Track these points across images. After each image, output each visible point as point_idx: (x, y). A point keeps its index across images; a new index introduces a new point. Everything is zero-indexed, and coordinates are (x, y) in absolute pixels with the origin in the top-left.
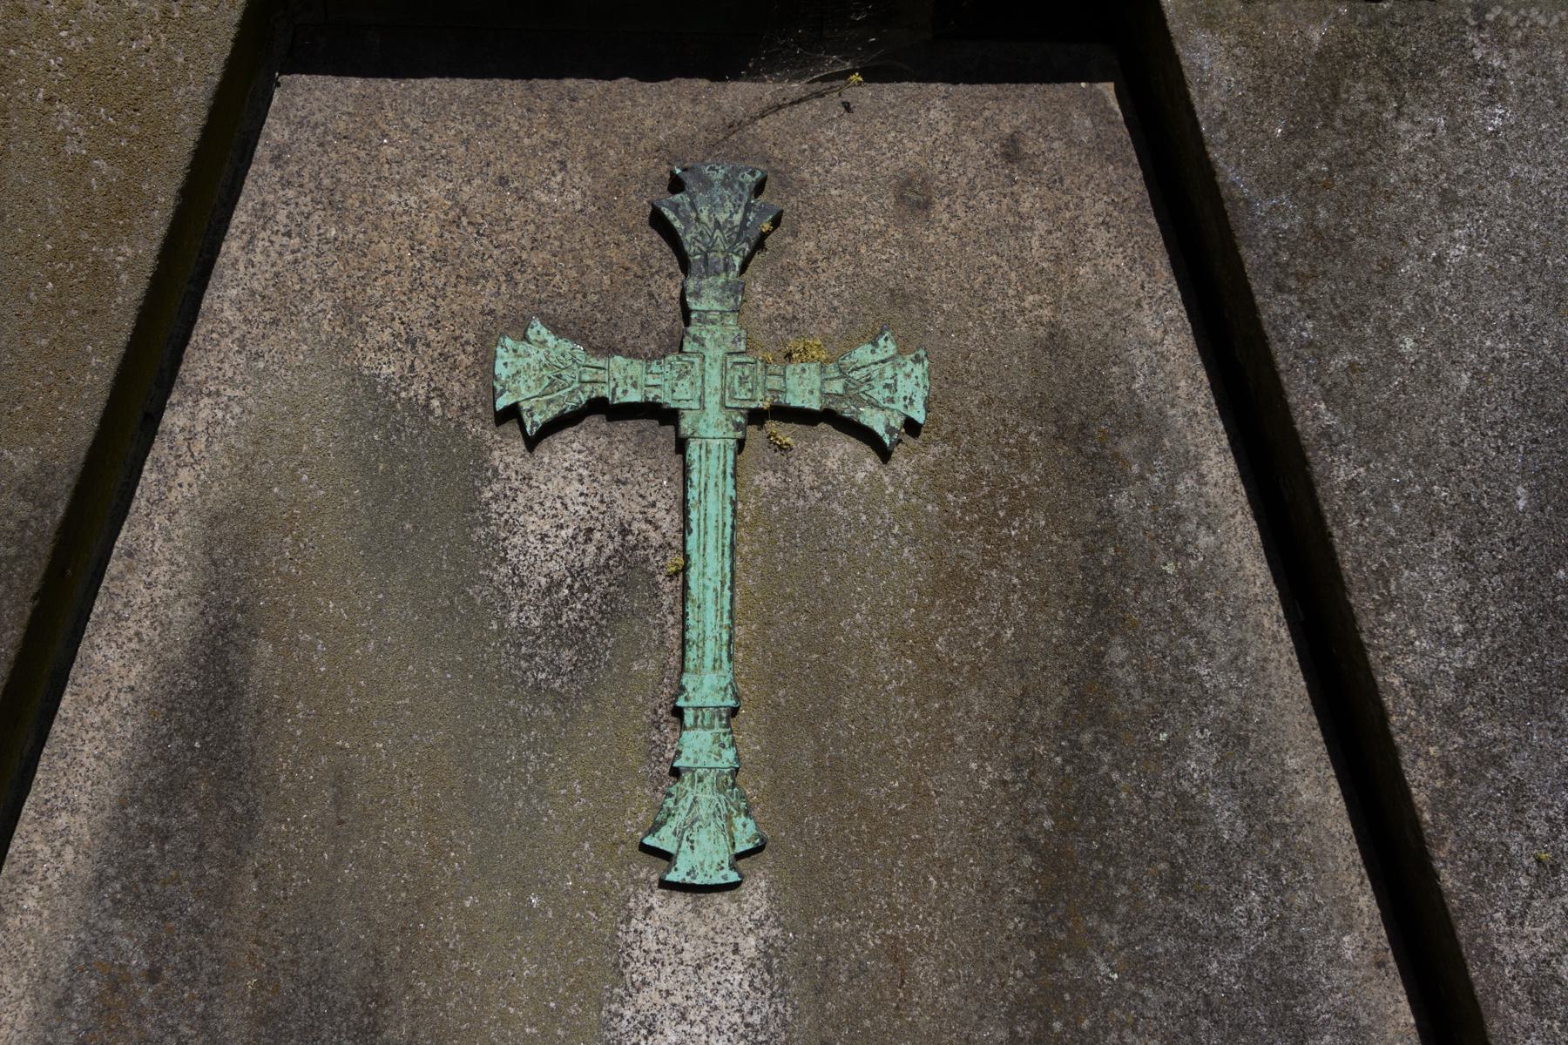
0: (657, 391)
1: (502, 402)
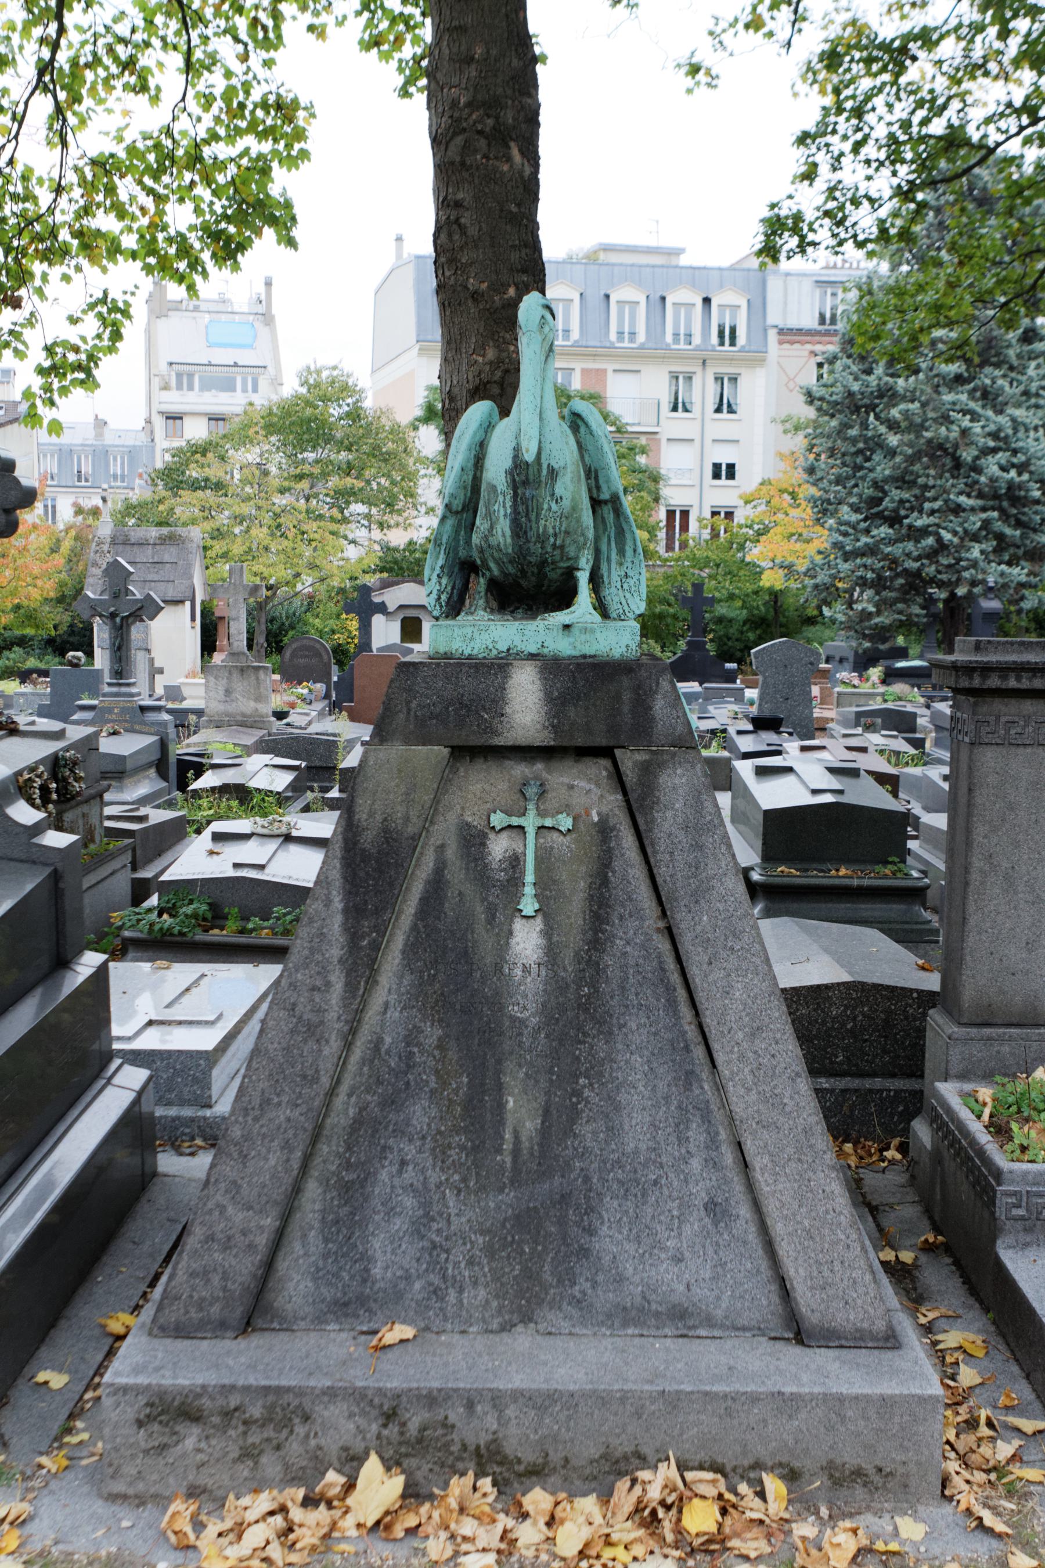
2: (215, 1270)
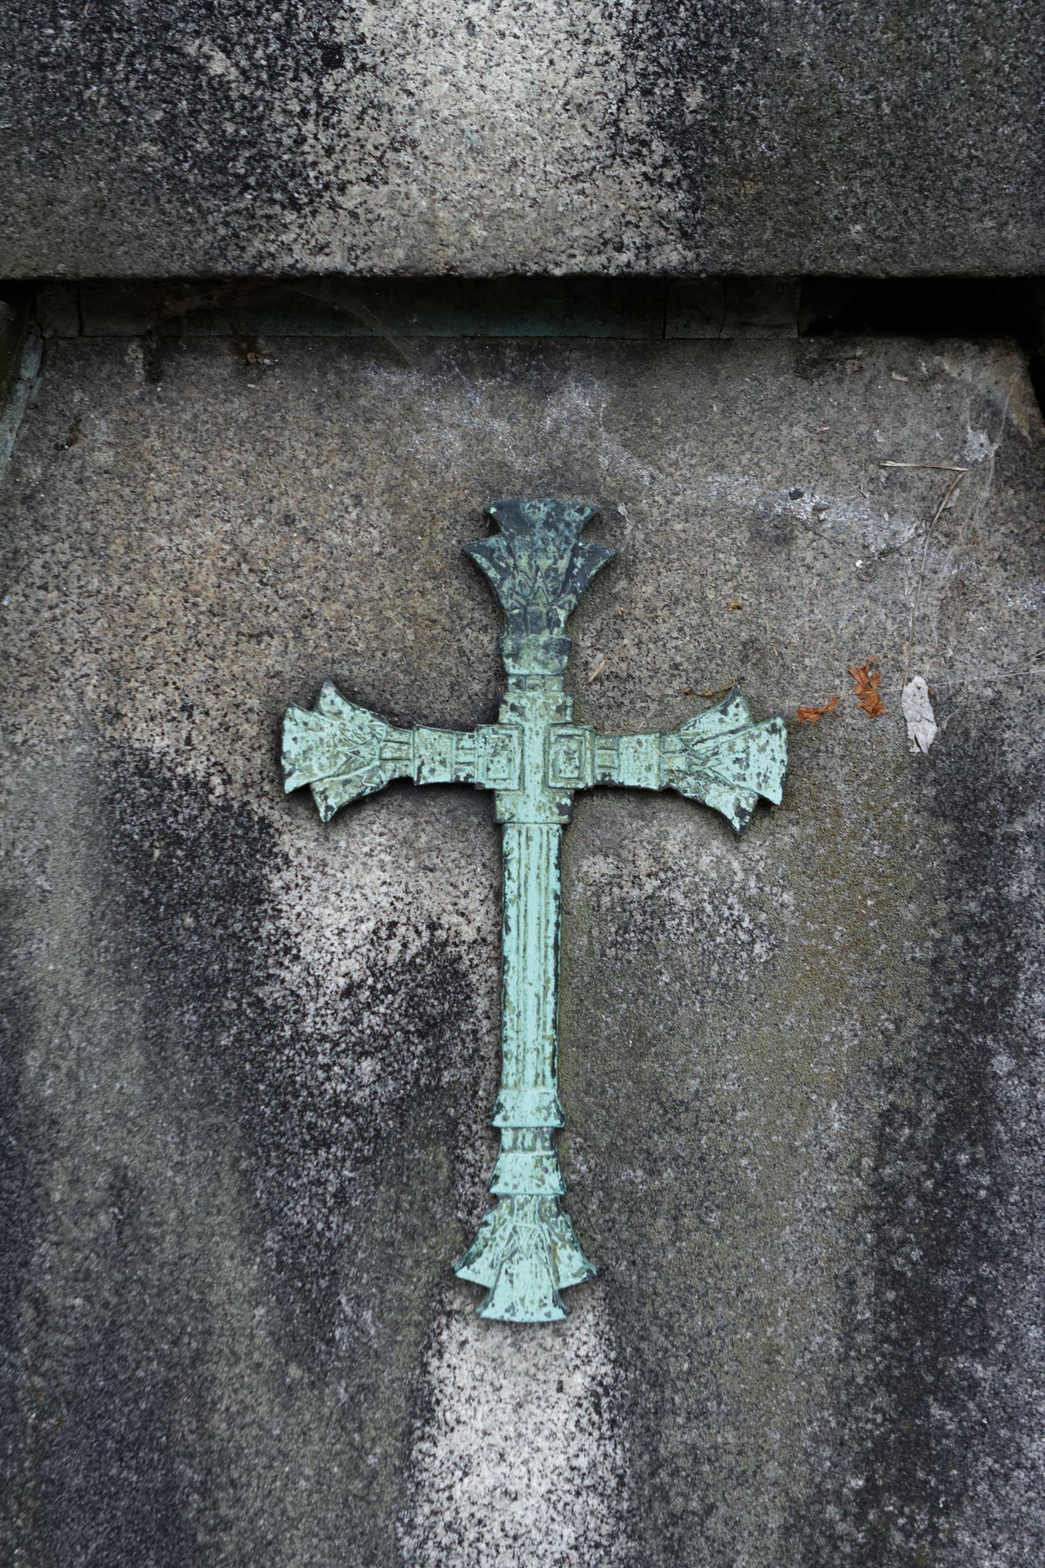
0: (468, 769)
1: (290, 785)
2: (12, 969)
